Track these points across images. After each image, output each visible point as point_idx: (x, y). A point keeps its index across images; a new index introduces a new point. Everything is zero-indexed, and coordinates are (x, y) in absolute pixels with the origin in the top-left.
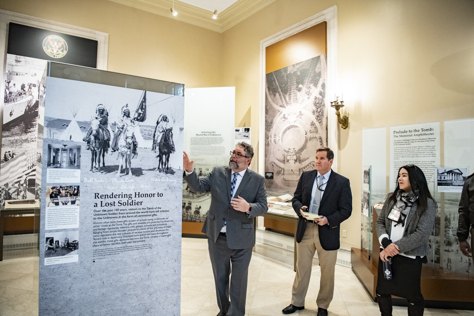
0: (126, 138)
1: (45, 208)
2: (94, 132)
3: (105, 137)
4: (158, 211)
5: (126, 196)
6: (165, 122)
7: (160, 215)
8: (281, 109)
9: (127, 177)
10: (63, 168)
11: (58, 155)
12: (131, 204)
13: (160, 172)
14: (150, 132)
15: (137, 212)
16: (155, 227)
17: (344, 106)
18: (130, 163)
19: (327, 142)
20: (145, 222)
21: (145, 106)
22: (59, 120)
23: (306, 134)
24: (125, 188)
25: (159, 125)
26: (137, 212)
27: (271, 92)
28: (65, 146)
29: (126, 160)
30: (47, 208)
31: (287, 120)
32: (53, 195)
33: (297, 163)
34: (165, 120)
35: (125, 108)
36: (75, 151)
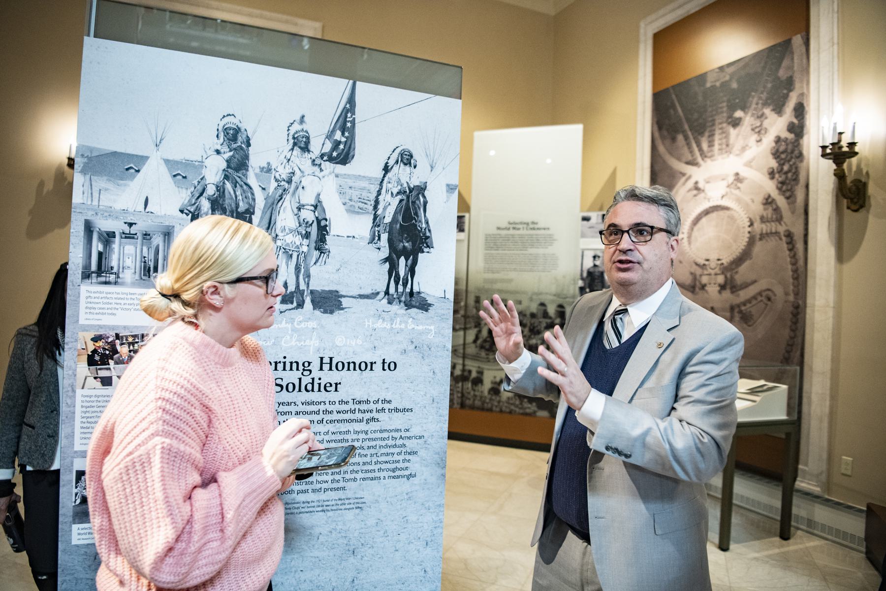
0: (299, 209)
1: (74, 391)
2: (211, 190)
3: (241, 204)
4: (383, 410)
5: (294, 365)
6: (407, 168)
7: (387, 421)
8: (689, 170)
9: (298, 315)
10: (123, 284)
11: (111, 250)
12: (309, 387)
13: (390, 303)
14: (365, 194)
15: (326, 412)
16: (373, 451)
17: (857, 153)
18: (308, 276)
19: (806, 242)
20: (346, 437)
21: (353, 122)
22: (115, 154)
23: (751, 225)
24: (293, 343)
25: (389, 175)
26: (326, 412)
27: (665, 133)
28: (131, 225)
29: (298, 269)
30: (79, 392)
31: (702, 195)
32: (97, 358)
33: (727, 294)
34: (408, 163)
35: (296, 127)
36: (158, 240)
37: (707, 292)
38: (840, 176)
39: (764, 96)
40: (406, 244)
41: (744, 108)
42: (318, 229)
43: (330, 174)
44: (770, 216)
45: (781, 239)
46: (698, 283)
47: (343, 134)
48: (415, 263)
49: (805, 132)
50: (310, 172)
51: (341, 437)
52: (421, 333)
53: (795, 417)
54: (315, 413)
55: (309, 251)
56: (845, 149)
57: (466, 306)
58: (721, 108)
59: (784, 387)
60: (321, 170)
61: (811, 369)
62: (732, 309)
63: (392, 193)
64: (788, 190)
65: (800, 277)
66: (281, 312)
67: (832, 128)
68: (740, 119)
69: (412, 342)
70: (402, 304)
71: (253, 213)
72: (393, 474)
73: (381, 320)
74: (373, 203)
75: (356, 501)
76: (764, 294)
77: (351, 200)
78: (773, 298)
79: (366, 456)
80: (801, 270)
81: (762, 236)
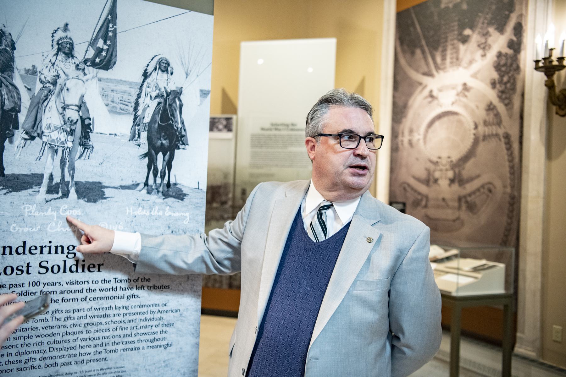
0: (64, 109)
3: (7, 102)
6: (165, 75)
8: (426, 80)
9: (64, 204)
13: (149, 193)
14: (126, 97)
15: (89, 290)
16: (133, 324)
19: (521, 143)
20: (108, 312)
21: (115, 32)
23: (476, 127)
24: (59, 229)
25: (148, 80)
26: (89, 290)
27: (406, 48)
29: (63, 162)
31: (435, 102)
33: (455, 187)
34: (165, 70)
35: (60, 34)
37: (439, 185)
38: (550, 86)
39: (489, 16)
40: (164, 142)
41: (472, 27)
42: (82, 127)
43: (93, 77)
44: (491, 120)
45: (500, 140)
46: (431, 178)
47: (105, 42)
48: (172, 158)
49: (522, 47)
50: (75, 76)
51: (103, 313)
52: (177, 220)
53: (512, 291)
54: (79, 291)
55: (73, 146)
56: (555, 63)
57: (234, 197)
58: (453, 27)
59: (502, 266)
60: (85, 74)
61: (525, 250)
62: (460, 199)
63: (151, 97)
64: (506, 98)
65: (516, 172)
66: (47, 201)
67: (544, 45)
68: (468, 37)
69: (169, 227)
70: (160, 194)
71: (19, 111)
72: (151, 345)
73: (141, 208)
74: (133, 105)
75: (117, 370)
76: (486, 187)
77: (113, 102)
78: (493, 190)
79: (126, 329)
80: (517, 166)
81: (485, 138)
